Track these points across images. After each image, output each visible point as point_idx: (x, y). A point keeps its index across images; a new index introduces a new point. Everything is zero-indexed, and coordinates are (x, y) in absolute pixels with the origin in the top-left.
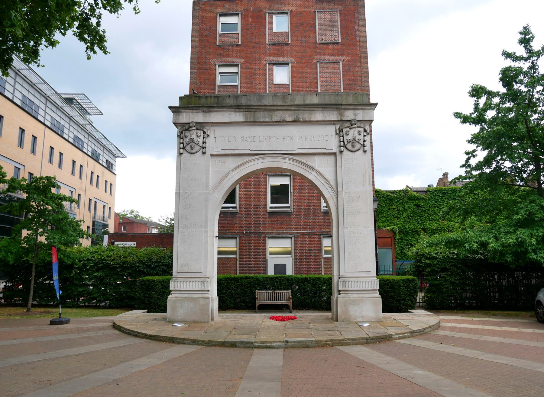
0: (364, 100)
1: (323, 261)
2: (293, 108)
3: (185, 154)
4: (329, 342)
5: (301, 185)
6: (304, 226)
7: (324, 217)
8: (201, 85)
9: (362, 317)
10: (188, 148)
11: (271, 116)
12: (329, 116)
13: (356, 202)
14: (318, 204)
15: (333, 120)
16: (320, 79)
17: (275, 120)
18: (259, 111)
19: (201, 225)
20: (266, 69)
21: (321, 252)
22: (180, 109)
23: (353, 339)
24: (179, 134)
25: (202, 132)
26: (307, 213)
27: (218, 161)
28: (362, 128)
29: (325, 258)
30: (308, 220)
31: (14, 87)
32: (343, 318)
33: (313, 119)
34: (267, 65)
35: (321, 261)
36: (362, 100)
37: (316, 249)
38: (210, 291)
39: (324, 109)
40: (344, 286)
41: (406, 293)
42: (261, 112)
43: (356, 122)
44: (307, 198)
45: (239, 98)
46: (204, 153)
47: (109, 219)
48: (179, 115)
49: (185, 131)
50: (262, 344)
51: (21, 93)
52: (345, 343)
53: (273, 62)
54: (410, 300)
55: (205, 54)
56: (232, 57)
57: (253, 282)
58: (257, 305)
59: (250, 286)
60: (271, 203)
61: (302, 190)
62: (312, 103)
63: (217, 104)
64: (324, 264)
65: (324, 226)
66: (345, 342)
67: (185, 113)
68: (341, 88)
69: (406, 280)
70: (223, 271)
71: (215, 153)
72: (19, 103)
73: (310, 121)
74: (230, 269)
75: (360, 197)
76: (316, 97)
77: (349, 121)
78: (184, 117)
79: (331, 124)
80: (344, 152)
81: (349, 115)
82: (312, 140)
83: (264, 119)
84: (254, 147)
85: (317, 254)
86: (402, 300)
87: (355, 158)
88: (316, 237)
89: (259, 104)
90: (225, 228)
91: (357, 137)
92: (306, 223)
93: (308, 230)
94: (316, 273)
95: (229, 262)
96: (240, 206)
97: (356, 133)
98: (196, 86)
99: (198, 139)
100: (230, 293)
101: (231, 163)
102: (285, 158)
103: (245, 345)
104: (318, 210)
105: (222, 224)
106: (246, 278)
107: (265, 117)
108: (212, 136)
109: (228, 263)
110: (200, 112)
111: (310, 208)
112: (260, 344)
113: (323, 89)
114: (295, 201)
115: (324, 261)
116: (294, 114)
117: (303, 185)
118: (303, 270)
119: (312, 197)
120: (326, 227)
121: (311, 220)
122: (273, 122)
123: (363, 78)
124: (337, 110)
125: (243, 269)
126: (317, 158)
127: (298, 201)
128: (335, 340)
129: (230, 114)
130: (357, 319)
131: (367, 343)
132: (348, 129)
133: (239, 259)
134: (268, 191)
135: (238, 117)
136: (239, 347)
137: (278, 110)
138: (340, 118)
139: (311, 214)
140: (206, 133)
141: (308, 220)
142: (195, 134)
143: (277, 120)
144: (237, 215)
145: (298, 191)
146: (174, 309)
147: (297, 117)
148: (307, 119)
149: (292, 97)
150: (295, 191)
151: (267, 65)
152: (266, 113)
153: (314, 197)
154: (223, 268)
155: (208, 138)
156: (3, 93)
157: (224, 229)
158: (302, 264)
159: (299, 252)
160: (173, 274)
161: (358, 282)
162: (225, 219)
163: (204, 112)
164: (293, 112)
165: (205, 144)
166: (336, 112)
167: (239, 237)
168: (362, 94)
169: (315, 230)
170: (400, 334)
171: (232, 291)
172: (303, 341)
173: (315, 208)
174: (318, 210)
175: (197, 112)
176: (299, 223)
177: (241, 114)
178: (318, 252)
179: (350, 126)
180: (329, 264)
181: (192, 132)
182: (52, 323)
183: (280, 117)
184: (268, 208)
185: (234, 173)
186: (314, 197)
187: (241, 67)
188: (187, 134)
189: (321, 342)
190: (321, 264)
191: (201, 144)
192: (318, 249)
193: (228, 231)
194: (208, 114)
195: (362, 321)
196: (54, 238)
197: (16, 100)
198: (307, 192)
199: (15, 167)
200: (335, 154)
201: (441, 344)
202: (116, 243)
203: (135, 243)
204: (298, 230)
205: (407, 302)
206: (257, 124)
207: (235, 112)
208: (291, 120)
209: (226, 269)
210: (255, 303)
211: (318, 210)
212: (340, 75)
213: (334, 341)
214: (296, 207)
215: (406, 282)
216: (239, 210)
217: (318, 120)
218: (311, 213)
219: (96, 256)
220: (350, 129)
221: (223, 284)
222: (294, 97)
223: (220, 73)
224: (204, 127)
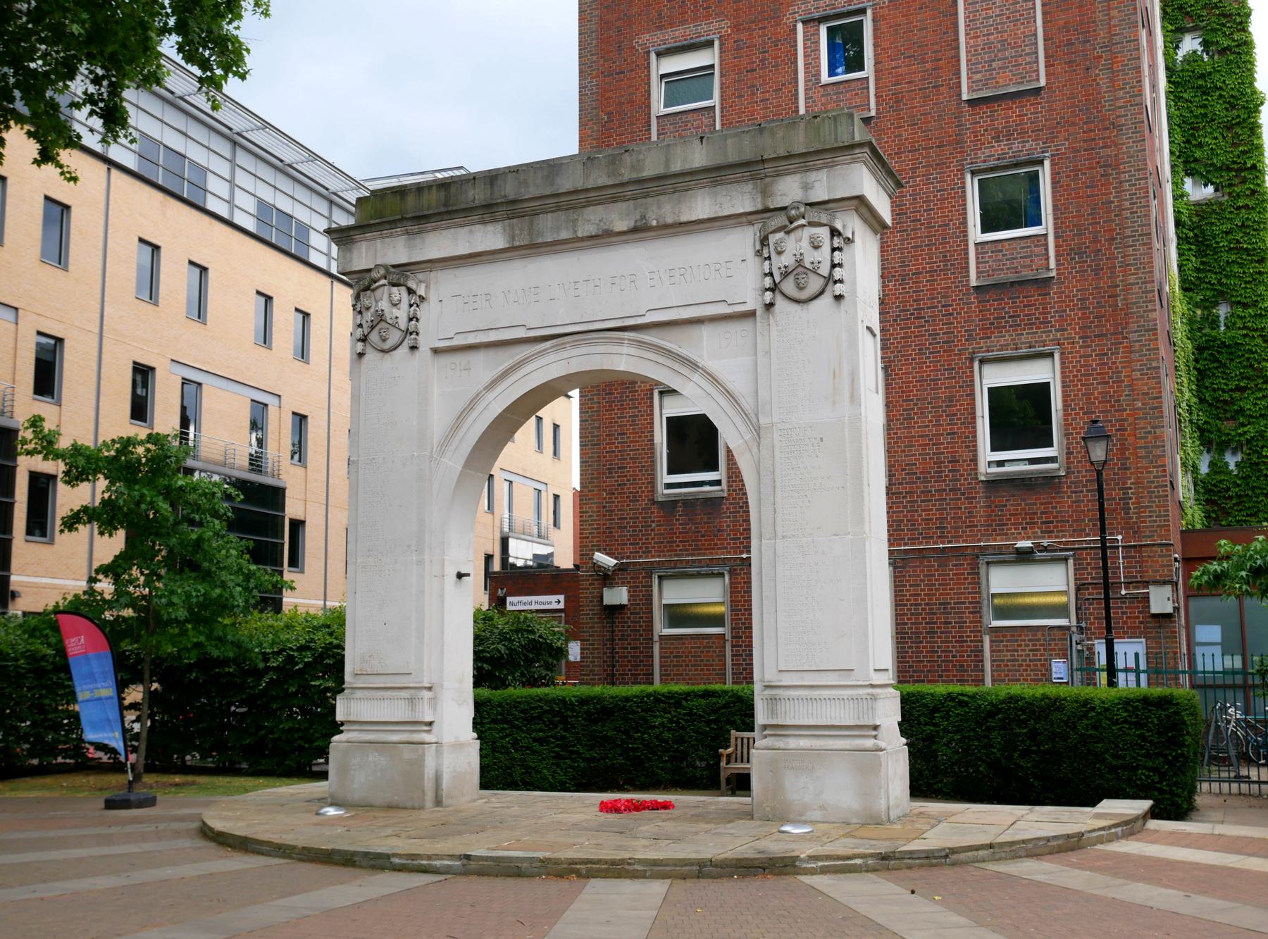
0: (839, 135)
1: (987, 639)
3: (371, 356)
4: (578, 866)
5: (912, 400)
6: (924, 529)
7: (987, 497)
8: (610, 121)
9: (823, 808)
10: (789, 287)
11: (575, 221)
13: (810, 456)
14: (966, 455)
15: (742, 211)
16: (967, 43)
17: (586, 234)
18: (543, 213)
19: (409, 546)
20: (796, 41)
21: (979, 612)
22: (352, 233)
23: (655, 863)
25: (403, 289)
26: (933, 486)
27: (453, 366)
28: (825, 225)
29: (995, 632)
30: (937, 510)
31: (231, 182)
32: (768, 809)
33: (684, 218)
34: (800, 26)
35: (982, 641)
37: (964, 603)
38: (435, 725)
39: (715, 183)
40: (773, 712)
41: (1137, 744)
42: (550, 215)
43: (802, 209)
44: (932, 440)
45: (499, 182)
46: (414, 348)
48: (350, 250)
50: (409, 862)
51: (254, 196)
52: (627, 871)
53: (816, 15)
54: (1154, 770)
55: (618, 24)
56: (695, 19)
57: (725, 706)
58: (723, 776)
60: (993, 449)
61: (915, 414)
62: (688, 167)
63: (445, 205)
64: (992, 651)
65: (988, 526)
66: (627, 867)
67: (364, 244)
68: (1037, 62)
69: (1138, 701)
70: (687, 675)
72: (250, 224)
74: (708, 670)
75: (821, 439)
77: (784, 208)
79: (741, 224)
81: (789, 190)
82: (688, 280)
83: (555, 236)
84: (536, 319)
85: (968, 617)
86: (1125, 767)
87: (808, 322)
88: (963, 565)
90: (691, 545)
91: (810, 257)
92: (932, 519)
93: (937, 543)
94: (968, 681)
95: (704, 647)
96: (732, 477)
97: (805, 245)
99: (394, 310)
100: (657, 737)
101: (483, 367)
102: (620, 342)
103: (372, 862)
104: (968, 475)
106: (707, 694)
107: (558, 229)
108: (433, 297)
109: (702, 652)
110: (398, 235)
111: (941, 472)
112: (404, 862)
113: (979, 76)
114: (897, 452)
115: (992, 641)
117: (918, 400)
118: (923, 671)
119: (948, 434)
120: (995, 530)
121: (946, 509)
122: (582, 239)
123: (1114, 13)
124: (754, 178)
127: (904, 451)
128: (599, 861)
129: (471, 232)
131: (698, 877)
132: (781, 235)
133: (732, 637)
134: (979, 413)
135: (490, 237)
136: (361, 867)
137: (590, 203)
139: (945, 490)
140: (415, 292)
141: (937, 510)
142: (386, 297)
143: (588, 234)
145: (904, 419)
146: (344, 770)
147: (643, 217)
148: (670, 220)
151: (800, 26)
152: (562, 216)
153: (954, 433)
154: (687, 666)
155: (424, 306)
156: (202, 205)
157: (687, 550)
158: (922, 652)
159: (912, 614)
160: (347, 677)
161: (837, 702)
163: (408, 234)
166: (750, 186)
167: (730, 572)
169: (959, 542)
170: (828, 858)
172: (510, 859)
173: (959, 471)
174: (968, 475)
175: (392, 236)
176: (908, 521)
177: (499, 226)
178: (972, 613)
179: (787, 223)
180: (1007, 651)
181: (378, 292)
182: (111, 804)
184: (982, 467)
185: (491, 396)
186: (954, 433)
187: (721, 49)
189: (555, 863)
190: (982, 651)
192: (969, 603)
193: (699, 554)
194: (418, 240)
196: (172, 592)
197: (240, 219)
198: (932, 421)
199: (252, 400)
200: (751, 314)
201: (913, 892)
202: (509, 599)
203: (562, 598)
204: (906, 544)
205: (1144, 774)
206: (541, 250)
207: (484, 223)
209: (696, 670)
210: (715, 769)
211: (970, 474)
212: (1035, 17)
213: (594, 863)
214: (896, 470)
215: (1137, 707)
216: (729, 490)
217: (700, 217)
218: (946, 485)
219: (318, 636)
220: (788, 233)
221: (634, 712)
222: (641, 157)
223: (663, 76)
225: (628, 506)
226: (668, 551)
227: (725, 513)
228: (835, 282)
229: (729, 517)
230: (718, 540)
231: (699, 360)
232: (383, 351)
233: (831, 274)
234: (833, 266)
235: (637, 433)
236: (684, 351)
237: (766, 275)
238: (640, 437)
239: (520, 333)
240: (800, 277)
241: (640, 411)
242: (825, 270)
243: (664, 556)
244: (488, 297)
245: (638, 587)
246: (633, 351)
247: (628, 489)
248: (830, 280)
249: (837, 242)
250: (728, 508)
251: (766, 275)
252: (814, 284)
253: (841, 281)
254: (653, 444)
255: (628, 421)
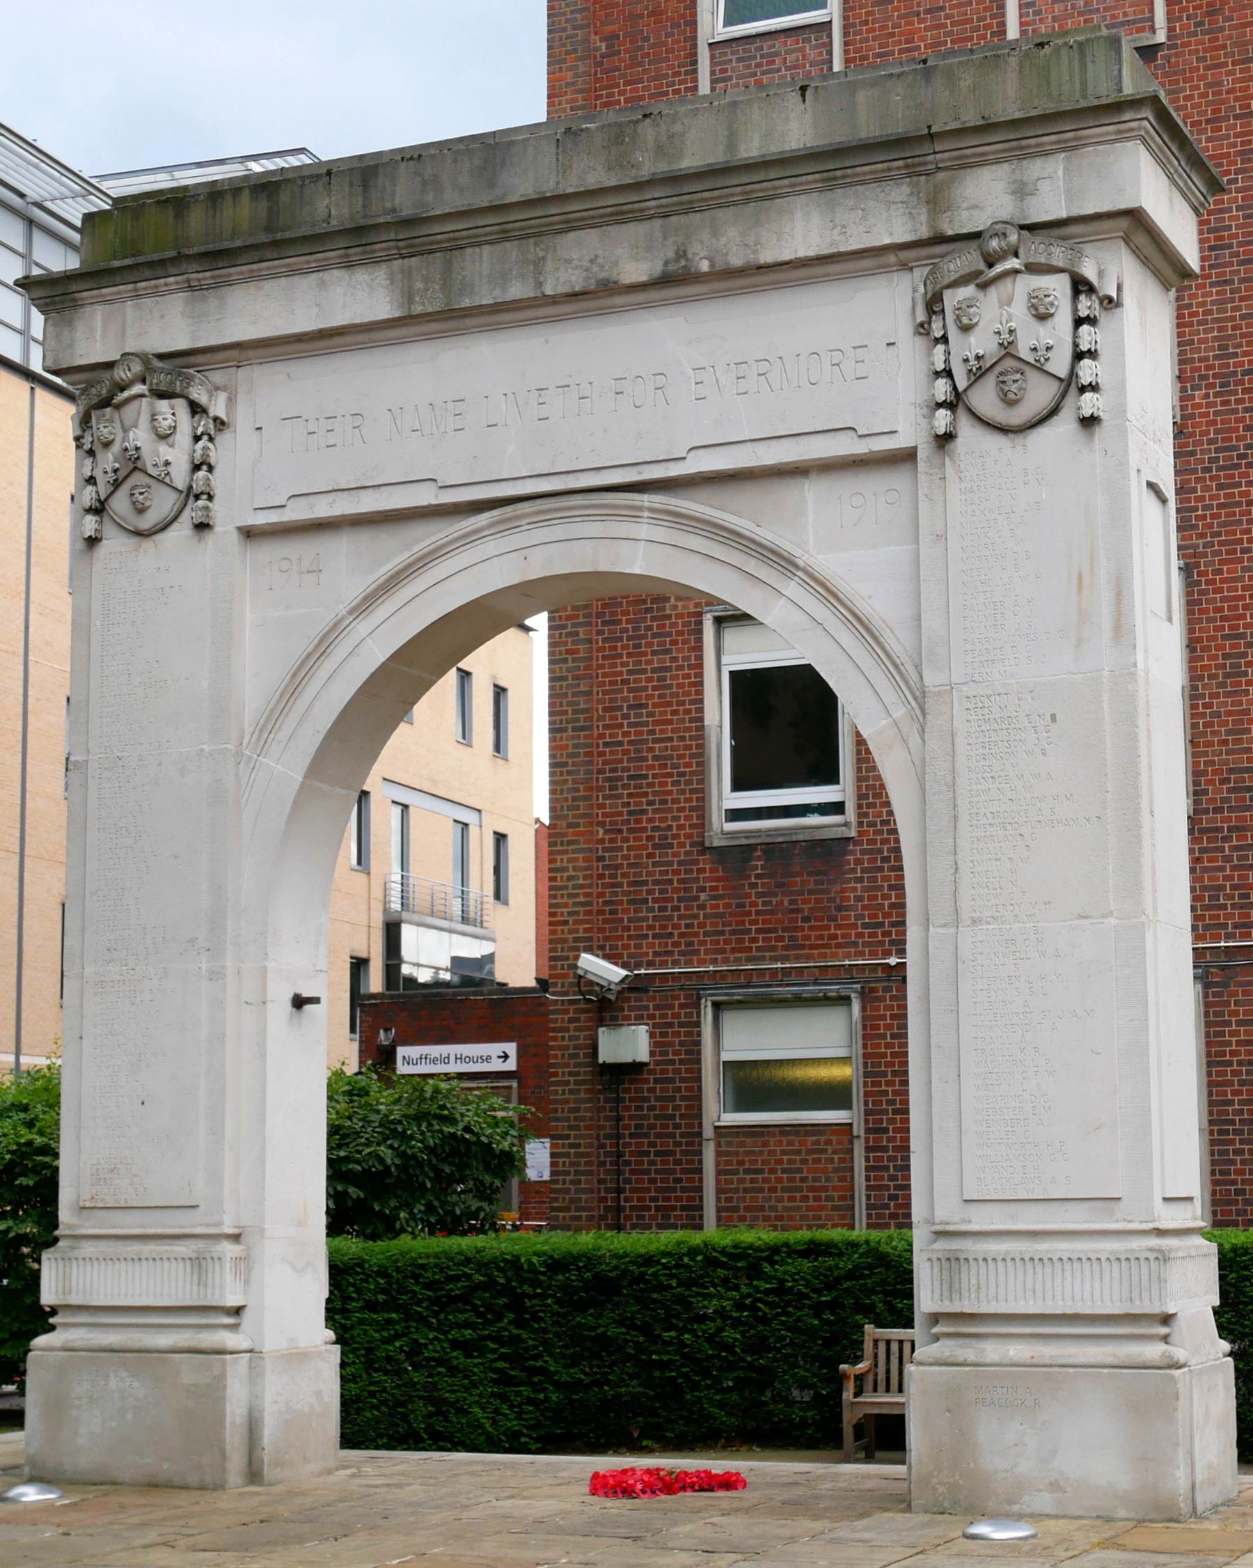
2: (653, 199)
3: (114, 544)
9: (1055, 1486)
11: (539, 263)
12: (864, 218)
15: (887, 241)
17: (562, 290)
18: (472, 245)
19: (193, 941)
24: (79, 433)
25: (181, 405)
28: (1062, 271)
32: (941, 1489)
33: (767, 257)
36: (1077, 86)
39: (830, 183)
40: (952, 1288)
43: (1013, 237)
45: (380, 181)
46: (202, 527)
47: (500, 908)
48: (70, 324)
49: (98, 412)
58: (849, 1419)
59: (835, 1299)
62: (775, 148)
71: (261, 519)
73: (759, 267)
75: (1053, 718)
76: (802, 107)
78: (98, 334)
79: (886, 269)
80: (960, 440)
83: (497, 292)
89: (483, 200)
91: (1029, 336)
96: (865, 796)
97: (1019, 311)
98: (582, 68)
100: (710, 1340)
102: (634, 514)
105: (758, 913)
106: (813, 1250)
107: (503, 279)
108: (243, 421)
109: (804, 1161)
110: (171, 292)
114: (1210, 744)
116: (665, 238)
122: (554, 300)
124: (912, 172)
125: (891, 1197)
126: (812, 492)
127: (1225, 742)
129: (322, 284)
130: (1025, 1499)
132: (968, 291)
133: (868, 1131)
137: (571, 226)
138: (931, 226)
142: (144, 420)
144: (846, 853)
145: (1227, 676)
146: (57, 1407)
147: (682, 254)
149: (663, 128)
150: (1201, 678)
152: (512, 250)
155: (223, 439)
157: (774, 948)
161: (1000, 1264)
162: (778, 885)
163: (191, 288)
164: (657, 223)
165: (202, 474)
167: (863, 995)
168: (1081, 45)
171: (720, 1330)
175: (156, 293)
176: (1233, 887)
177: (380, 274)
181: (129, 411)
183: (586, 263)
185: (362, 627)
188: (104, 427)
191: (180, 476)
193: (797, 958)
194: (212, 301)
195: (1052, 1512)
200: (907, 457)
202: (402, 1051)
203: (511, 1048)
204: (1229, 937)
206: (470, 322)
207: (350, 265)
208: (644, 278)
209: (792, 1199)
216: (860, 824)
217: (801, 254)
220: (983, 286)
222: (678, 128)
224: (189, 379)
225: (649, 856)
226: (734, 950)
227: (854, 871)
228: (1083, 390)
229: (860, 880)
230: (838, 927)
231: (797, 552)
232: (139, 534)
233: (1073, 373)
234: (1079, 356)
235: (669, 704)
236: (766, 535)
237: (937, 374)
238: (675, 712)
239: (426, 497)
240: (1008, 378)
241: (674, 659)
242: (1060, 364)
243: (726, 961)
244: (358, 421)
245: (671, 1025)
246: (660, 533)
247: (650, 820)
248: (1072, 385)
249: (1086, 306)
250: (857, 862)
251: (937, 374)
252: (1039, 394)
253: (1094, 388)
254: (702, 728)
255: (649, 680)
